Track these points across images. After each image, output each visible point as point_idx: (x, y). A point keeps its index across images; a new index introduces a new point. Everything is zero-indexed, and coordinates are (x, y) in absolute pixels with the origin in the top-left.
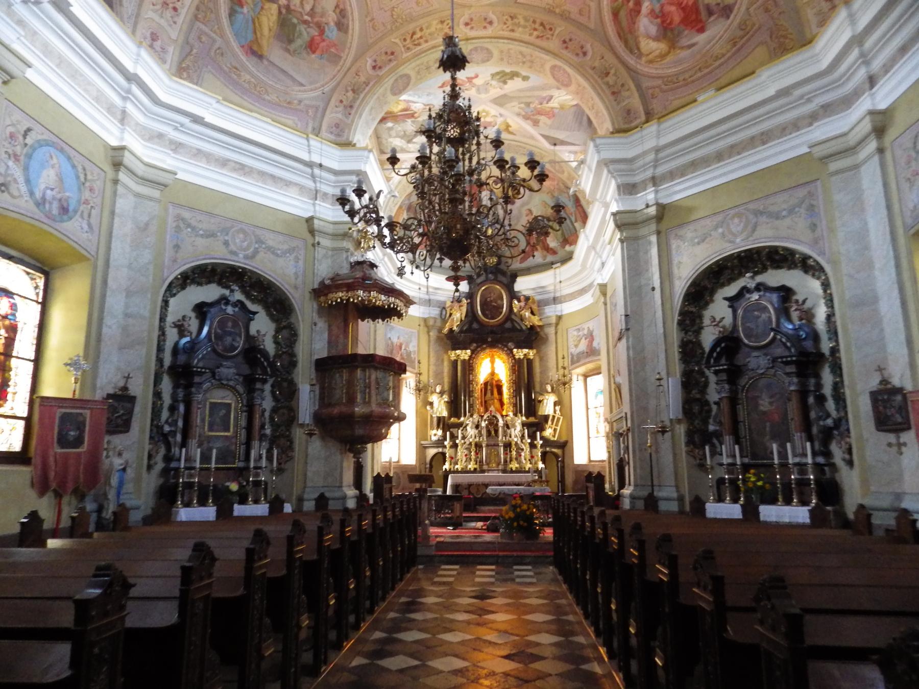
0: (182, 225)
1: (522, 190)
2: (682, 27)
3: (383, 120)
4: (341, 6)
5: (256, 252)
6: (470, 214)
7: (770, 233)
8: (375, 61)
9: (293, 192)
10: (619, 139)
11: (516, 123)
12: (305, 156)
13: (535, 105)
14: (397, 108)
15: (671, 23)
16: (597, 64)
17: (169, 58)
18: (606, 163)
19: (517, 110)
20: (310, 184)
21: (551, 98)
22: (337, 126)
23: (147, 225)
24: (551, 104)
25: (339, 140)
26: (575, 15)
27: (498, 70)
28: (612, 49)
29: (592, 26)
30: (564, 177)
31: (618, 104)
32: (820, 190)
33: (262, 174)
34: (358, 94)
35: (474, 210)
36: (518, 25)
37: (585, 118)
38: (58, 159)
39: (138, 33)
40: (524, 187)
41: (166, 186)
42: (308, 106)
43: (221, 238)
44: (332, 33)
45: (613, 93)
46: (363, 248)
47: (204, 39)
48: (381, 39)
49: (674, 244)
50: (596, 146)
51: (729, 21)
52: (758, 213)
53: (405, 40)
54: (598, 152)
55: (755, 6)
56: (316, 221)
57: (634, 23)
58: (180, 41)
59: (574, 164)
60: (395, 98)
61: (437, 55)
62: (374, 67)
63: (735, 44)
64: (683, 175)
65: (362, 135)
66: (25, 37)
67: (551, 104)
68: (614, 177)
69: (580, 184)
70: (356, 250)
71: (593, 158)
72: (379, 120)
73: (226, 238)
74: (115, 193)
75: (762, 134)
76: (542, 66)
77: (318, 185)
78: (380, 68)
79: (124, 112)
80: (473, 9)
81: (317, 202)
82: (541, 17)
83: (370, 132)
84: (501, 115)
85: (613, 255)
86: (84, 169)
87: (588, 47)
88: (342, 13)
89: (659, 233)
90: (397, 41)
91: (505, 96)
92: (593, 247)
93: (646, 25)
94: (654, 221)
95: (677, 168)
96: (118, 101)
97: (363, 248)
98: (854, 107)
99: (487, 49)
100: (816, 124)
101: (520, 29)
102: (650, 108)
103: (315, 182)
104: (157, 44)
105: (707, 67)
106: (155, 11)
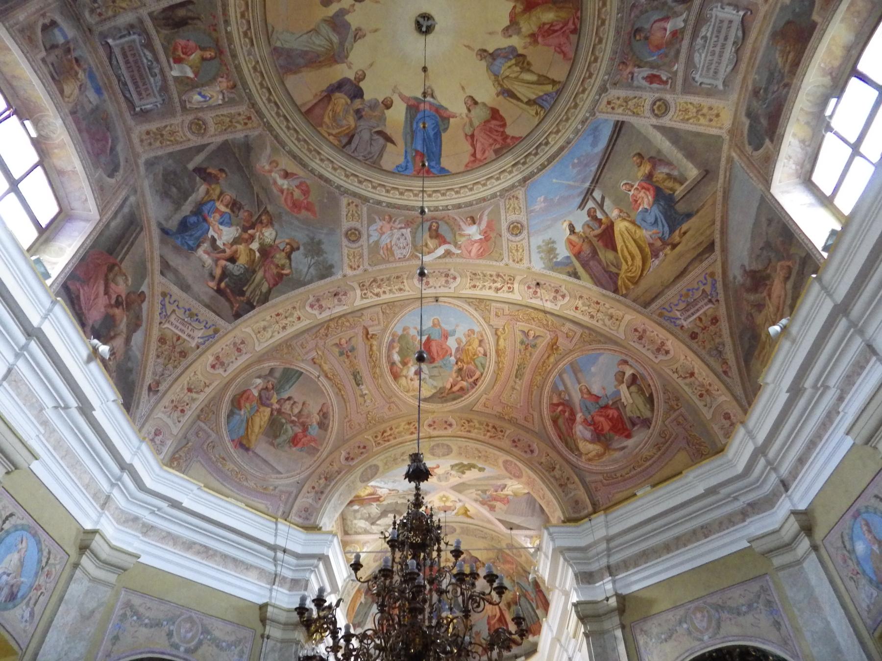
0: (129, 613)
1: (482, 603)
2: (612, 433)
3: (351, 503)
4: (325, 410)
5: (200, 643)
6: (430, 627)
7: (736, 630)
8: (349, 453)
9: (252, 576)
10: (571, 528)
11: (474, 508)
12: (270, 540)
13: (491, 492)
14: (364, 493)
15: (602, 430)
16: (543, 460)
17: (165, 450)
18: (560, 551)
19: (474, 496)
20: (270, 568)
21: (505, 486)
22: (306, 510)
23: (93, 612)
24: (505, 492)
25: (307, 523)
26: (522, 421)
27: (457, 462)
28: (554, 447)
29: (537, 430)
30: (522, 560)
31: (566, 495)
32: (771, 584)
33: (225, 557)
34: (330, 482)
35: (434, 622)
36: (474, 427)
37: (537, 505)
38: (28, 544)
39: (145, 430)
40: (483, 599)
41: (125, 570)
42: (282, 492)
43: (166, 628)
44: (314, 431)
45: (561, 485)
46: (315, 639)
47: (201, 433)
48: (354, 436)
49: (641, 640)
50: (550, 534)
51: (651, 430)
52: (719, 608)
53: (376, 437)
54: (553, 540)
55: (669, 420)
56: (270, 609)
57: (572, 429)
58: (180, 435)
59: (532, 551)
60: (364, 485)
61: (404, 469)
62: (347, 459)
63: (659, 449)
64: (636, 565)
65: (329, 521)
66: (43, 435)
67: (505, 492)
68: (571, 565)
69: (538, 571)
70: (306, 642)
71: (548, 547)
72: (348, 502)
73: (172, 628)
74: (71, 577)
75: (702, 527)
76: (496, 460)
77: (279, 569)
78: (352, 459)
79: (108, 497)
80: (435, 414)
81: (275, 587)
82: (492, 422)
83: (337, 515)
84: (460, 501)
85: (580, 650)
86: (49, 553)
87: (535, 446)
88: (324, 415)
89: (623, 627)
90: (370, 438)
91: (463, 484)
92: (557, 639)
93: (581, 430)
94: (616, 613)
95: (630, 558)
96: (105, 486)
97: (315, 639)
98: (777, 506)
99: (448, 446)
100: (748, 520)
101: (476, 431)
102: (596, 499)
103: (276, 565)
104: (158, 439)
105: (639, 466)
106: (164, 413)
